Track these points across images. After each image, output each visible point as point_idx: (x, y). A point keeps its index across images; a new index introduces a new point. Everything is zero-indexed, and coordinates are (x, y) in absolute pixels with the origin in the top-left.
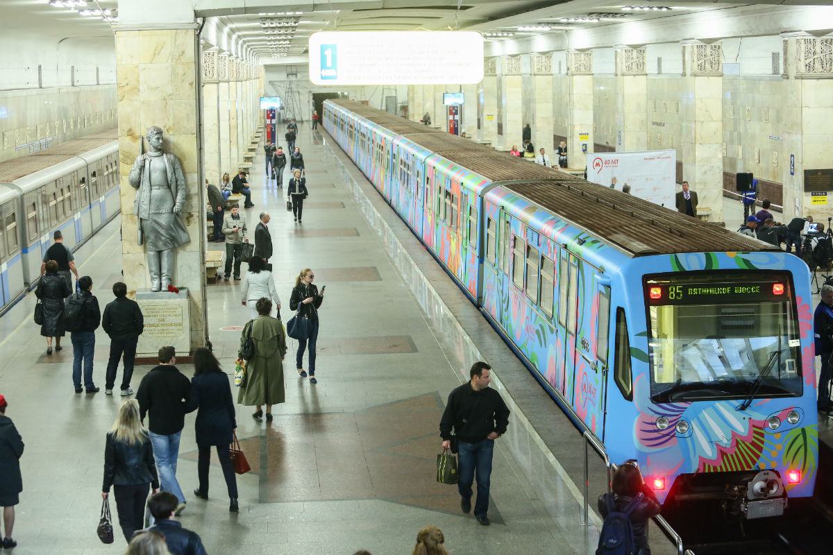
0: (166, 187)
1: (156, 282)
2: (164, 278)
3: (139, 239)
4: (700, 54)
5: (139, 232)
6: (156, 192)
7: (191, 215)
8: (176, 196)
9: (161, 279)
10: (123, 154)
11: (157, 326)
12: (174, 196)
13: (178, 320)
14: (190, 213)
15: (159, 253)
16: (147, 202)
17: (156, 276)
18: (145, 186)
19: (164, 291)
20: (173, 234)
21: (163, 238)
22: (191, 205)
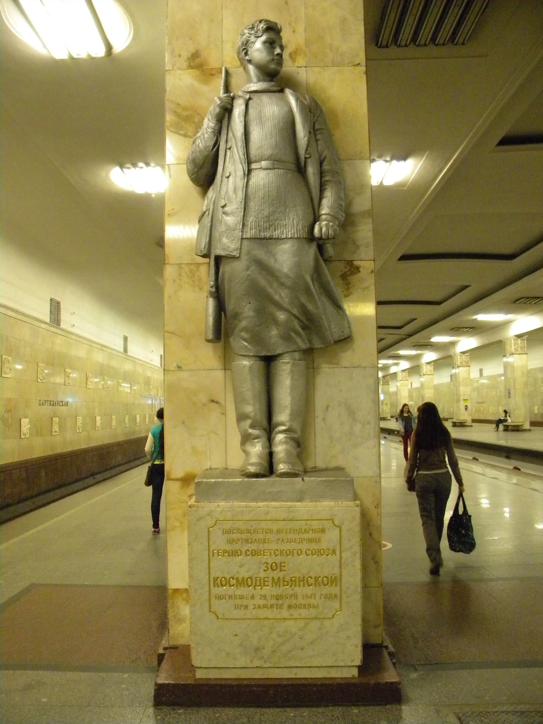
0: (293, 167)
1: (257, 449)
2: (280, 437)
3: (211, 320)
4: (515, 344)
5: (211, 302)
6: (261, 177)
7: (353, 269)
8: (321, 199)
9: (270, 440)
10: (175, 113)
11: (263, 583)
12: (316, 202)
13: (327, 566)
14: (350, 263)
15: (268, 361)
16: (234, 205)
17: (255, 432)
18: (231, 166)
20: (310, 307)
21: (282, 316)
22: (354, 243)
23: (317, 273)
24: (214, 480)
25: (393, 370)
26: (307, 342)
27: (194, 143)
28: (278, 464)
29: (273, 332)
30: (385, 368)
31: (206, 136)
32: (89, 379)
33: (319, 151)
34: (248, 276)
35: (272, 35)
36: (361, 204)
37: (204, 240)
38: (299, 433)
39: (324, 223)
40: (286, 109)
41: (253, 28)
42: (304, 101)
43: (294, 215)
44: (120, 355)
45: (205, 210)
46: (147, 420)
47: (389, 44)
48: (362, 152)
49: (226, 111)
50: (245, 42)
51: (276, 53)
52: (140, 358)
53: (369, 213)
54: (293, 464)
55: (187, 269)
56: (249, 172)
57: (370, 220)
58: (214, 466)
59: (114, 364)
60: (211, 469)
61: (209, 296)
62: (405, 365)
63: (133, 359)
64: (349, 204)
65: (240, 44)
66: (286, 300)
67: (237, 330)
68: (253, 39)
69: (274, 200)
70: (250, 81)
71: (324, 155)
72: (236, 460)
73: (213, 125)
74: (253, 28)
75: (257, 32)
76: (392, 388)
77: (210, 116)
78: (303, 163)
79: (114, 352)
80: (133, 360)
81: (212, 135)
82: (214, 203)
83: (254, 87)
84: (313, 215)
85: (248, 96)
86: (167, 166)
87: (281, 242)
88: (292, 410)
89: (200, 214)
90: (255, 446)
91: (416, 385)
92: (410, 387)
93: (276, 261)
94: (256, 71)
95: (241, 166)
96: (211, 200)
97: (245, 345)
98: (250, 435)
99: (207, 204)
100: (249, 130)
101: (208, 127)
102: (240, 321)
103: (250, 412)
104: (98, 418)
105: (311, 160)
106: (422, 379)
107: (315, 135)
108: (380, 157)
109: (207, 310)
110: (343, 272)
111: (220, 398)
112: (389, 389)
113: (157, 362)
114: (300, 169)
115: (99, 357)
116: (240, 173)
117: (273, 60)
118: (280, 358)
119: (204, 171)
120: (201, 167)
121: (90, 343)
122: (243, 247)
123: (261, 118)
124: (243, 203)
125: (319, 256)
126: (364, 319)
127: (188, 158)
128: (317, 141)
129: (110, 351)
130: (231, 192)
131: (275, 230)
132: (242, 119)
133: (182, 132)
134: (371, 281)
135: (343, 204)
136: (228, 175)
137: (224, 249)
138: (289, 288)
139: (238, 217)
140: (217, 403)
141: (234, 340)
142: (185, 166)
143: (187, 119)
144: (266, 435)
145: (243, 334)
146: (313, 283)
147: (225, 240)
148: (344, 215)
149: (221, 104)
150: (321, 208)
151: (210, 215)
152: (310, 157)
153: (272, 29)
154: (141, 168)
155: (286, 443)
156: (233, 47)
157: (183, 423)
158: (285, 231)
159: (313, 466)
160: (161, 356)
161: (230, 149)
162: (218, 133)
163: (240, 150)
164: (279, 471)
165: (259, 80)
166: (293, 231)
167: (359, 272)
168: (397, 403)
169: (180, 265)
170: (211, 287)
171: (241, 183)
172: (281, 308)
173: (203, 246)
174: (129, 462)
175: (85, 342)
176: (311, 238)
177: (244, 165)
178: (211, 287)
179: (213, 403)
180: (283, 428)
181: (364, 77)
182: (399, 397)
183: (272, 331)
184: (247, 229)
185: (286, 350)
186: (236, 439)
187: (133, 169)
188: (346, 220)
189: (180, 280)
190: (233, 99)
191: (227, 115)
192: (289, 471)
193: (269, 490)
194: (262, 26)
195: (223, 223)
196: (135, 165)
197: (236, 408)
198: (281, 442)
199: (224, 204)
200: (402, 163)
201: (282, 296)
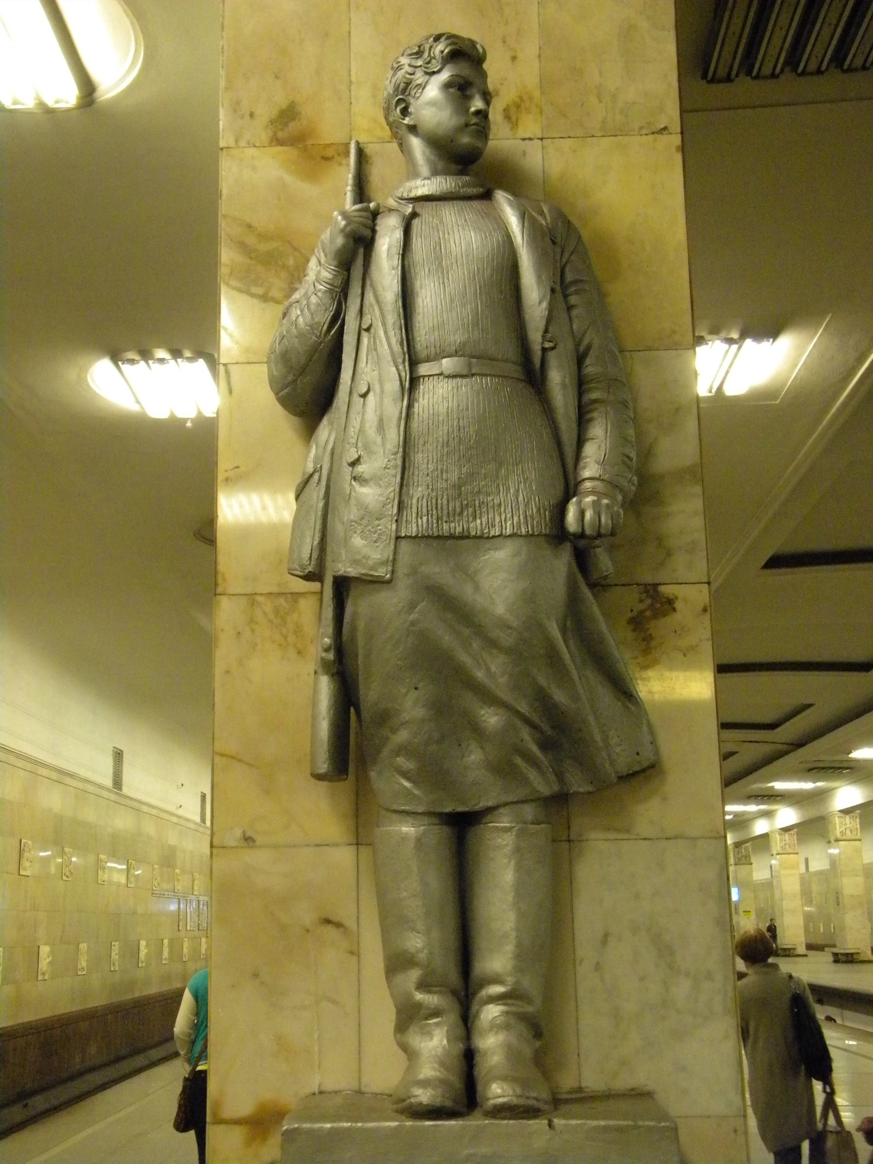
0: (515, 371)
1: (435, 1042)
2: (491, 1013)
3: (324, 727)
5: (325, 687)
6: (440, 396)
8: (580, 442)
9: (467, 1020)
10: (242, 246)
14: (651, 590)
15: (461, 827)
16: (380, 461)
18: (372, 369)
19: (502, 1111)
20: (559, 696)
21: (491, 719)
22: (660, 540)
23: (575, 617)
24: (329, 1126)
25: (760, 827)
26: (553, 778)
27: (285, 315)
28: (488, 1084)
29: (473, 757)
30: (741, 822)
31: (314, 300)
32: (26, 855)
33: (575, 331)
34: (413, 624)
35: (465, 69)
36: (676, 450)
37: (308, 540)
38: (538, 1001)
39: (589, 499)
40: (497, 237)
41: (419, 54)
42: (540, 218)
43: (519, 483)
44: (105, 794)
45: (311, 470)
46: (166, 954)
47: (734, 73)
48: (674, 332)
49: (359, 245)
50: (402, 86)
51: (473, 109)
52: (153, 801)
53: (695, 473)
54: (525, 1084)
55: (268, 607)
56: (412, 385)
57: (698, 489)
58: (330, 1085)
59: (89, 815)
60: (321, 1092)
61: (320, 670)
62: (787, 816)
63: (135, 805)
64: (647, 454)
65: (390, 90)
66: (503, 680)
67: (385, 753)
68: (419, 77)
69: (470, 448)
70: (414, 174)
71: (586, 342)
72: (383, 1073)
73: (330, 276)
74: (419, 54)
75: (428, 63)
76: (759, 872)
77: (322, 254)
78: (538, 374)
79: (91, 788)
80: (136, 807)
81: (327, 301)
82: (332, 454)
83: (423, 187)
84: (562, 480)
85: (409, 209)
86: (222, 369)
87: (488, 544)
88: (518, 946)
89: (299, 480)
90: (430, 1034)
91: (818, 864)
92: (802, 869)
93: (477, 587)
94: (427, 151)
95: (394, 369)
96: (325, 447)
97: (405, 787)
98: (419, 1006)
99: (316, 457)
100: (412, 284)
101: (318, 280)
102: (394, 731)
103: (419, 951)
104: (45, 950)
105: (559, 352)
106: (834, 851)
107: (565, 296)
108: (715, 331)
109: (314, 703)
110: (635, 613)
111: (345, 914)
112: (750, 874)
113: (191, 810)
114: (533, 377)
115: (53, 800)
116: (392, 385)
117: (467, 125)
118: (489, 817)
119: (308, 381)
120: (302, 371)
121: (29, 766)
122: (400, 557)
123: (439, 259)
124: (400, 455)
125: (579, 577)
126: (686, 709)
127: (272, 351)
128: (569, 308)
129: (80, 785)
130: (371, 431)
131: (475, 518)
132: (396, 261)
133: (260, 291)
134: (701, 632)
135: (633, 455)
136: (365, 390)
137: (355, 562)
138: (508, 651)
139: (387, 487)
140: (339, 925)
141: (380, 773)
142: (264, 368)
143: (269, 260)
144: (457, 1006)
145: (400, 760)
146: (565, 641)
147: (357, 541)
148: (635, 478)
149: (348, 229)
150: (581, 464)
151: (324, 483)
152: (553, 348)
153: (465, 55)
154: (162, 361)
155: (506, 1027)
156: (374, 96)
157: (256, 975)
158: (497, 519)
159: (576, 1085)
160: (203, 797)
161: (368, 330)
162: (340, 293)
163: (392, 334)
164: (492, 1102)
165: (435, 173)
166: (516, 519)
167: (674, 610)
168: (773, 908)
169: (252, 598)
170: (327, 650)
171: (393, 409)
172: (490, 699)
173: (306, 555)
174: (119, 1059)
175: (20, 763)
176: (558, 534)
177: (401, 367)
178: (327, 650)
179: (330, 928)
180: (497, 989)
181: (678, 157)
182: (777, 895)
183: (471, 752)
184: (411, 514)
185: (504, 798)
186: (382, 1013)
187: (142, 363)
188: (640, 490)
189: (253, 631)
190: (375, 214)
191: (361, 251)
192: (515, 1101)
193: (466, 1152)
194: (441, 47)
195: (353, 502)
196: (146, 355)
197: (386, 941)
198: (494, 1027)
199: (356, 456)
200: (766, 345)
201: (493, 670)
